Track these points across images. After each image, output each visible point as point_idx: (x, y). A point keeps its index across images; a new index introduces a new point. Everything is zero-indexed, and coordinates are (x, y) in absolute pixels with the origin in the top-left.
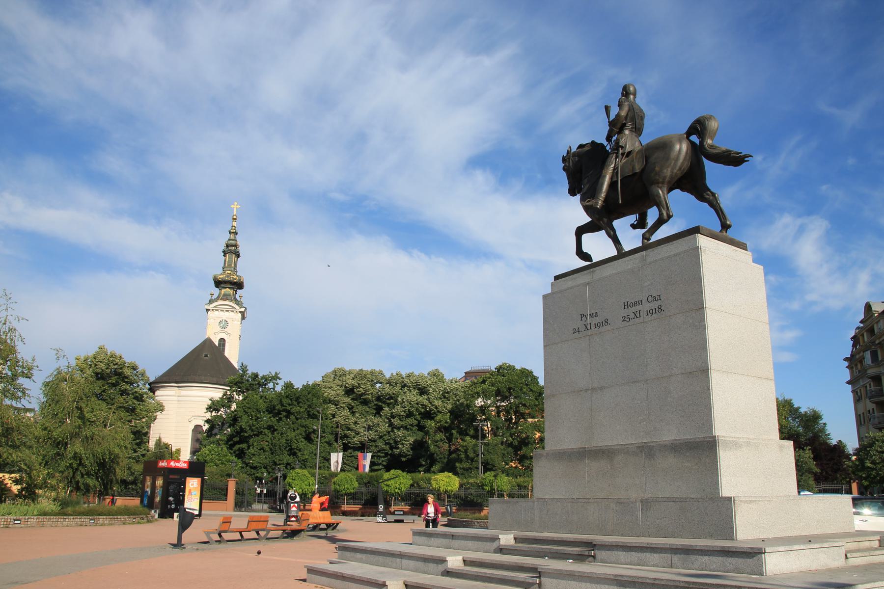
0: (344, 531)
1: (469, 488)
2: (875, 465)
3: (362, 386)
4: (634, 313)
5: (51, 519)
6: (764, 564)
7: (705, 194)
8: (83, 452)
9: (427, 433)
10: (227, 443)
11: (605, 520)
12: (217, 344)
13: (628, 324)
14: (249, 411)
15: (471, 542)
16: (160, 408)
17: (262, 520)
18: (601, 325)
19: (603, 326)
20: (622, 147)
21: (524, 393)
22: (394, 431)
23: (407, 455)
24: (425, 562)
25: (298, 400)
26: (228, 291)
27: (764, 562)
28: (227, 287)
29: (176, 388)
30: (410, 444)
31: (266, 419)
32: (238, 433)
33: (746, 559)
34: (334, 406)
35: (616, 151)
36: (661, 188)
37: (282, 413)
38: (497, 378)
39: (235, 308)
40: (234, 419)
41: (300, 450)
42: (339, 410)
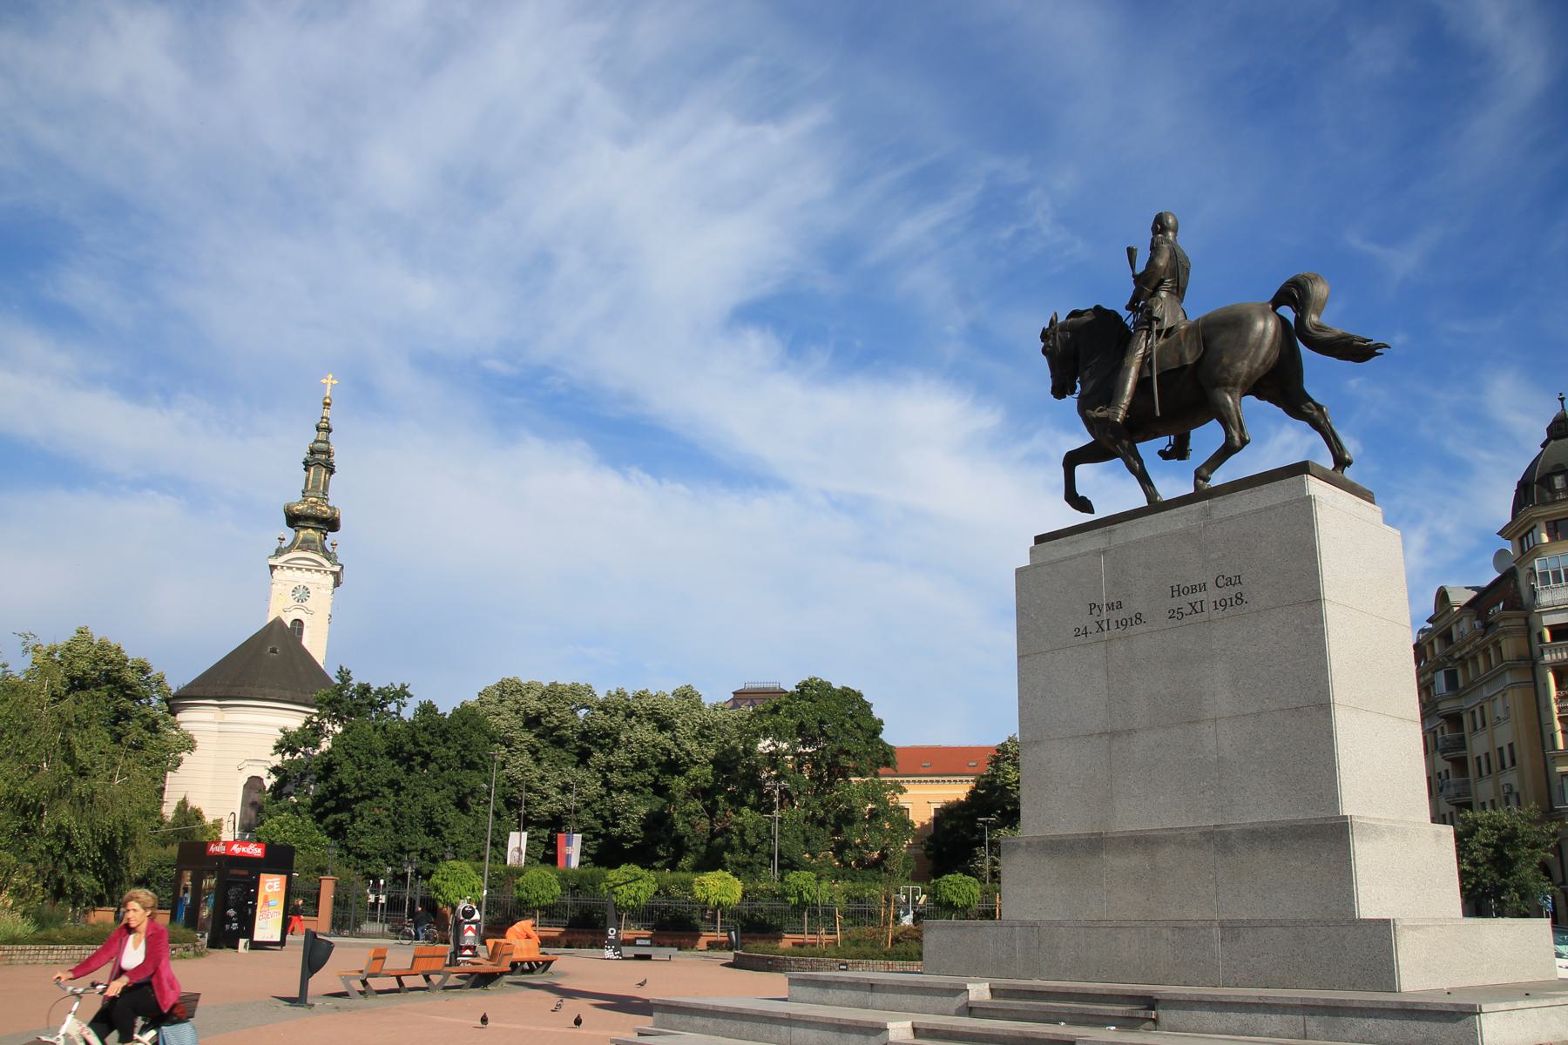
0: (563, 975)
1: (756, 900)
2: (1475, 867)
3: (555, 713)
4: (1191, 604)
5: (25, 950)
6: (1479, 1032)
7: (1303, 406)
8: (74, 825)
9: (671, 799)
10: (312, 811)
11: (1152, 958)
12: (289, 626)
13: (1179, 623)
14: (356, 753)
15: (909, 996)
16: (189, 744)
17: (437, 954)
18: (1129, 623)
19: (1132, 625)
20: (1158, 320)
21: (847, 732)
22: (611, 794)
23: (634, 838)
24: (841, 1031)
25: (444, 735)
26: (311, 533)
27: (1478, 1029)
28: (309, 527)
29: (217, 708)
30: (640, 819)
31: (388, 769)
32: (334, 793)
33: (1445, 1024)
34: (504, 747)
35: (1147, 327)
36: (1230, 393)
37: (414, 757)
38: (800, 704)
39: (322, 565)
40: (328, 768)
41: (447, 826)
42: (513, 755)
